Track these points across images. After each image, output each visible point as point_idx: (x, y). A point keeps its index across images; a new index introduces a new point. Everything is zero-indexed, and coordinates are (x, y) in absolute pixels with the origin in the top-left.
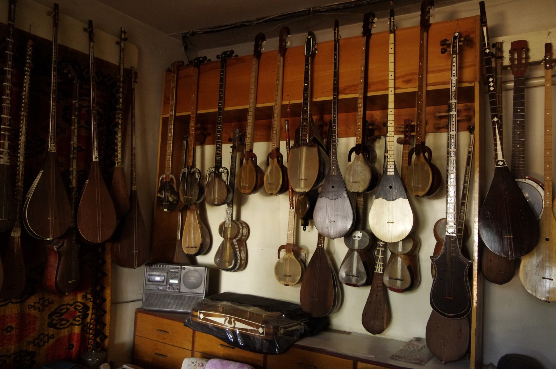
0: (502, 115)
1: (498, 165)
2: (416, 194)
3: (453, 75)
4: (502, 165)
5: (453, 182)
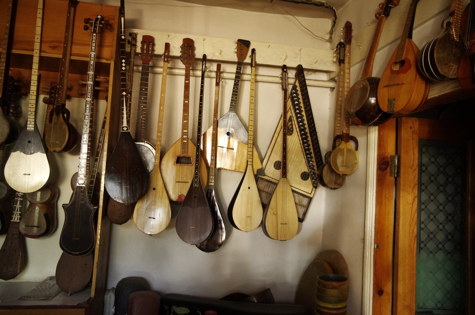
0: (132, 91)
1: (123, 130)
2: (54, 150)
3: (92, 51)
4: (126, 130)
5: (86, 141)
